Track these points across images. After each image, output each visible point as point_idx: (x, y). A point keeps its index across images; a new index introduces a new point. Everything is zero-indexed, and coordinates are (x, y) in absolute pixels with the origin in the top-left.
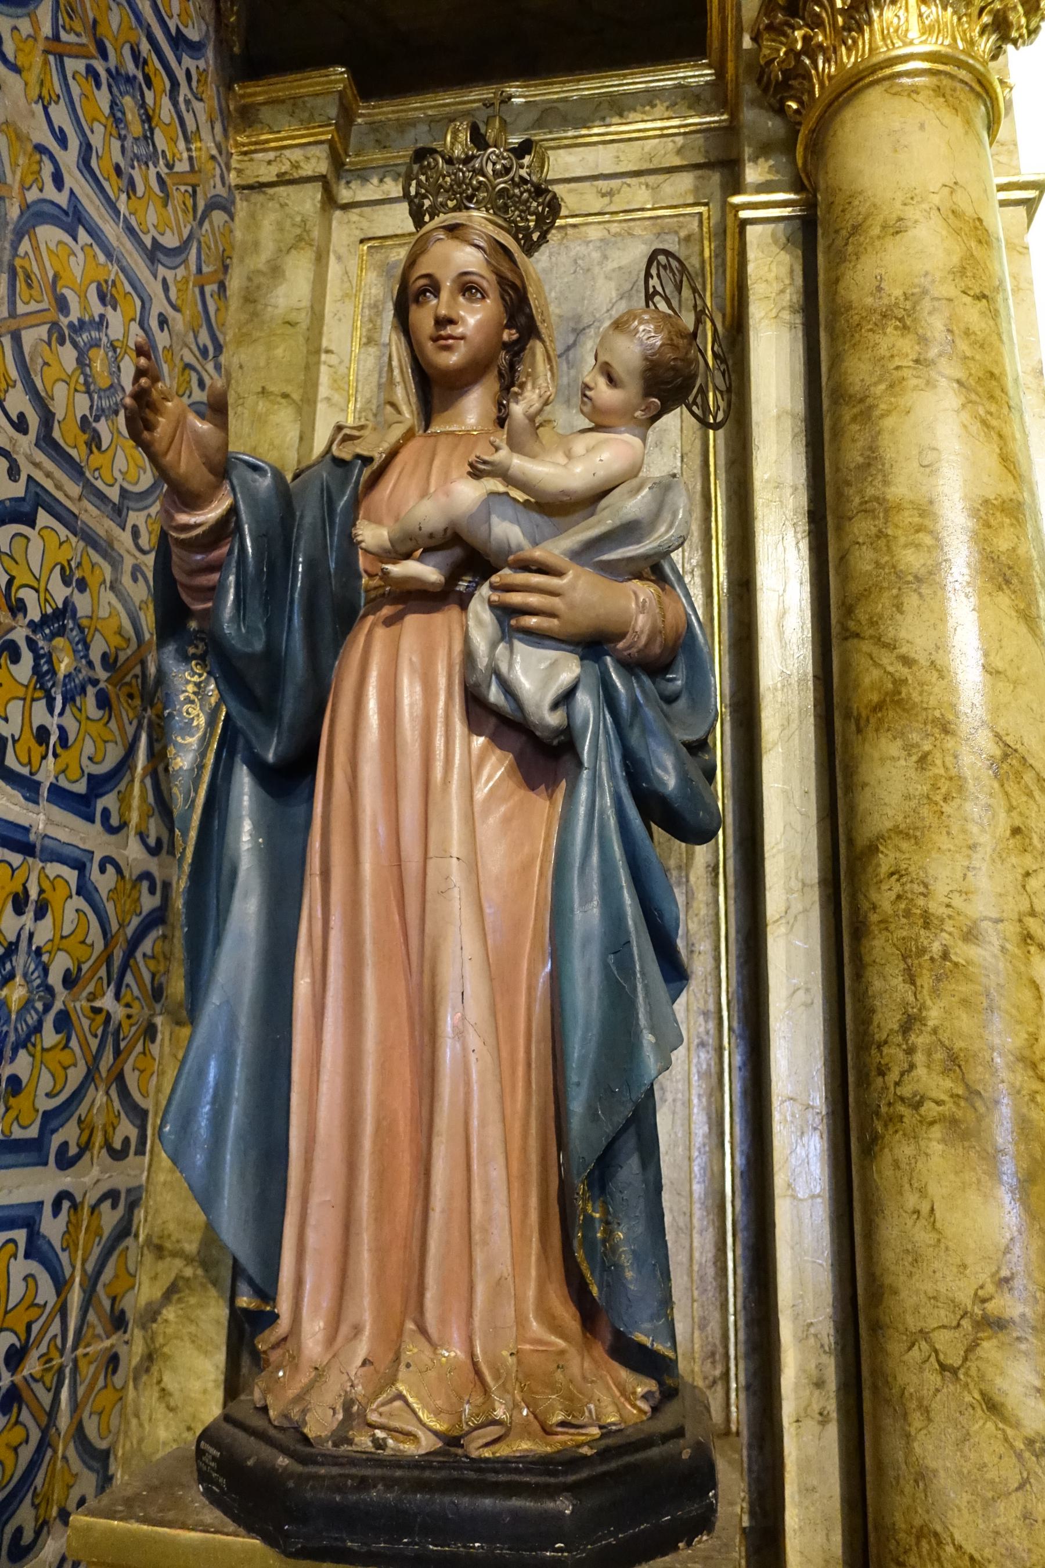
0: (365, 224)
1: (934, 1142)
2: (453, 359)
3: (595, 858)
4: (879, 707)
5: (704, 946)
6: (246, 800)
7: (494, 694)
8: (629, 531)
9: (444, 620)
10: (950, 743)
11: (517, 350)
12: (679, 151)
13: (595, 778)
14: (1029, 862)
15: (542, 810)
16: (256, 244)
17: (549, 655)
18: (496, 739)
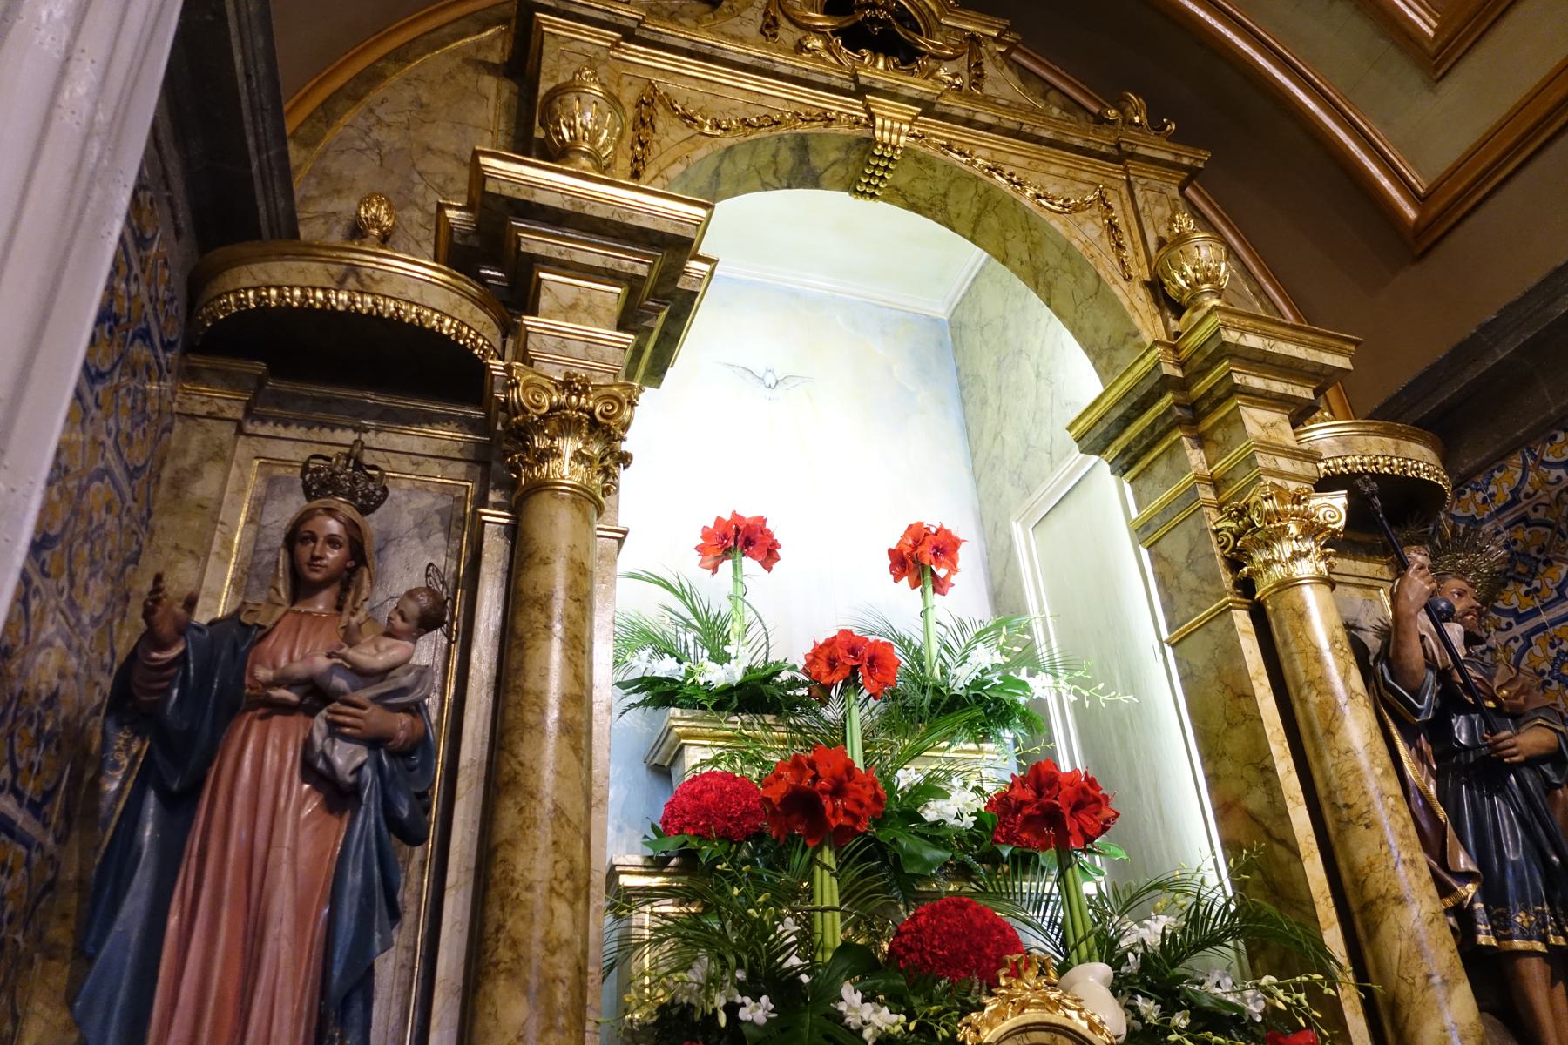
0: (260, 448)
1: (502, 982)
2: (317, 576)
3: (362, 850)
4: (507, 784)
5: (412, 909)
6: (151, 810)
7: (320, 764)
8: (403, 691)
9: (296, 722)
10: (533, 803)
11: (353, 572)
12: (461, 451)
13: (368, 807)
14: (558, 857)
15: (337, 827)
16: (185, 452)
17: (352, 747)
18: (316, 787)
